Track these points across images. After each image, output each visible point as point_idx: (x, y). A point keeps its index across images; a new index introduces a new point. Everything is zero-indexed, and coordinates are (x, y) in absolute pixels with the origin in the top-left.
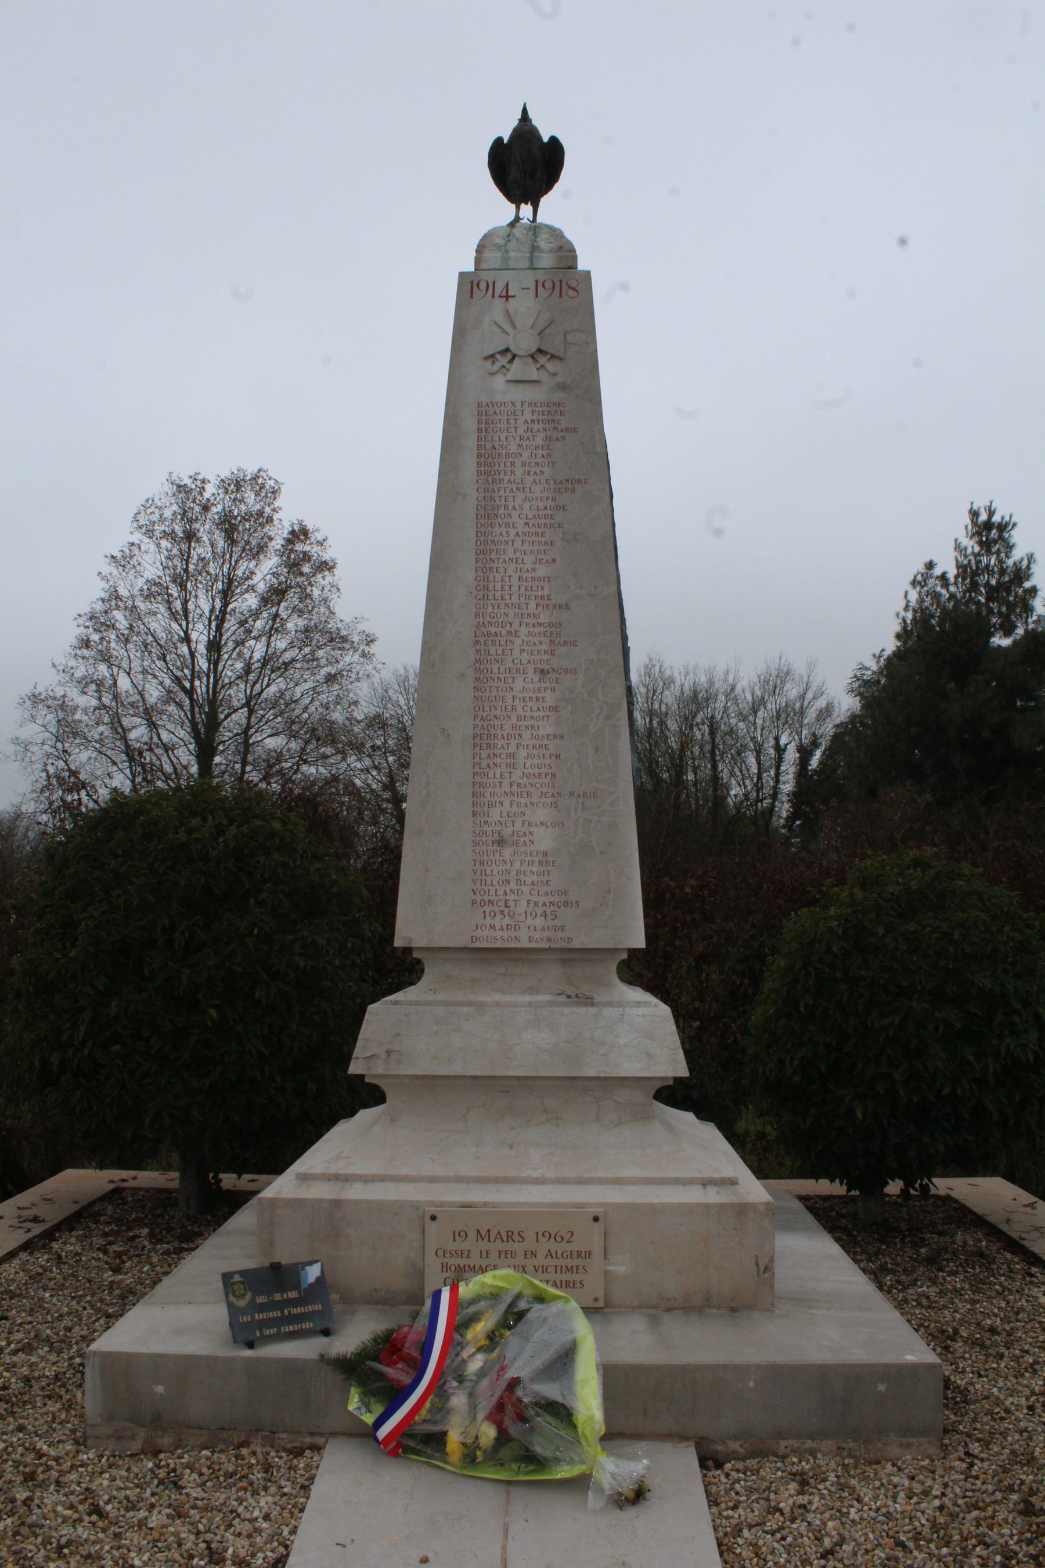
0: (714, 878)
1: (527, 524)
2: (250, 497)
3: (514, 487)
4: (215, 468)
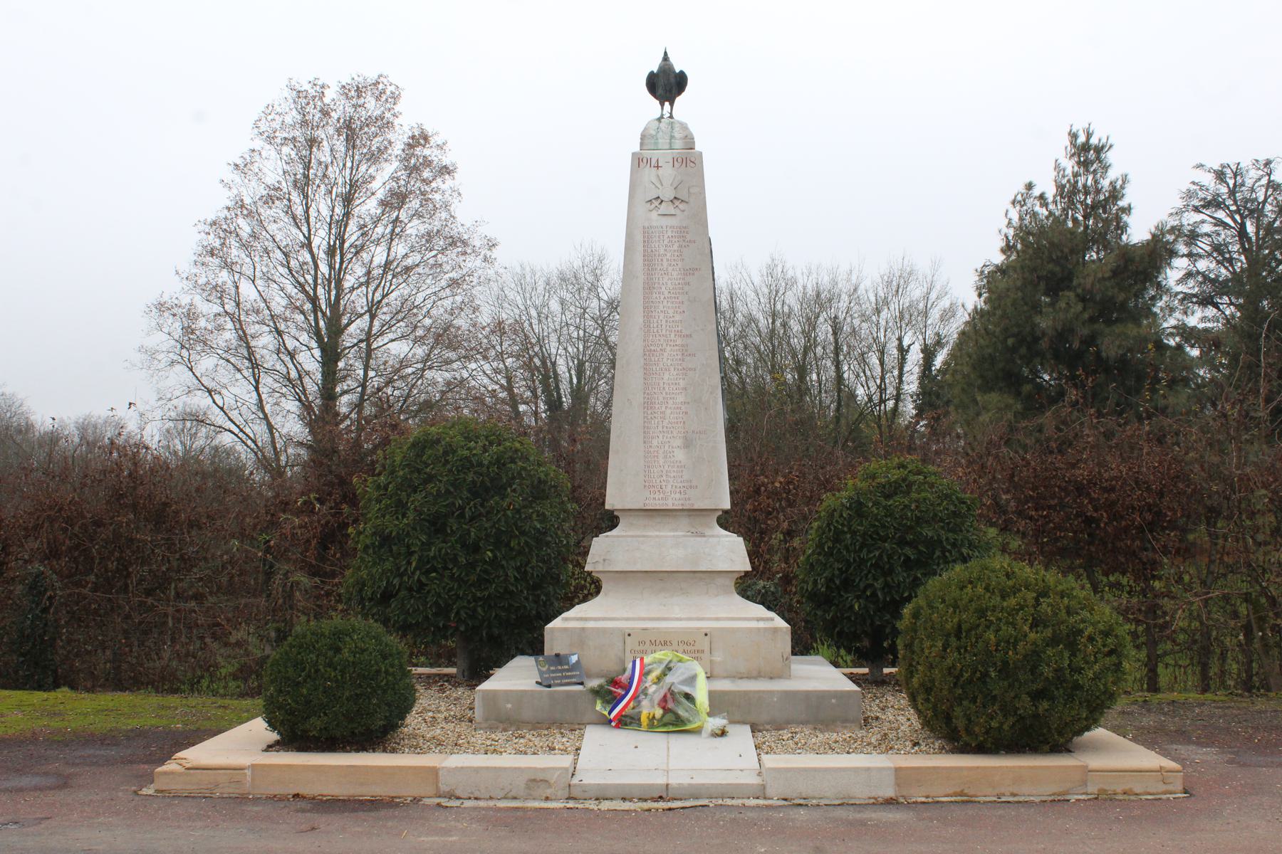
2: (370, 103)
4: (335, 74)
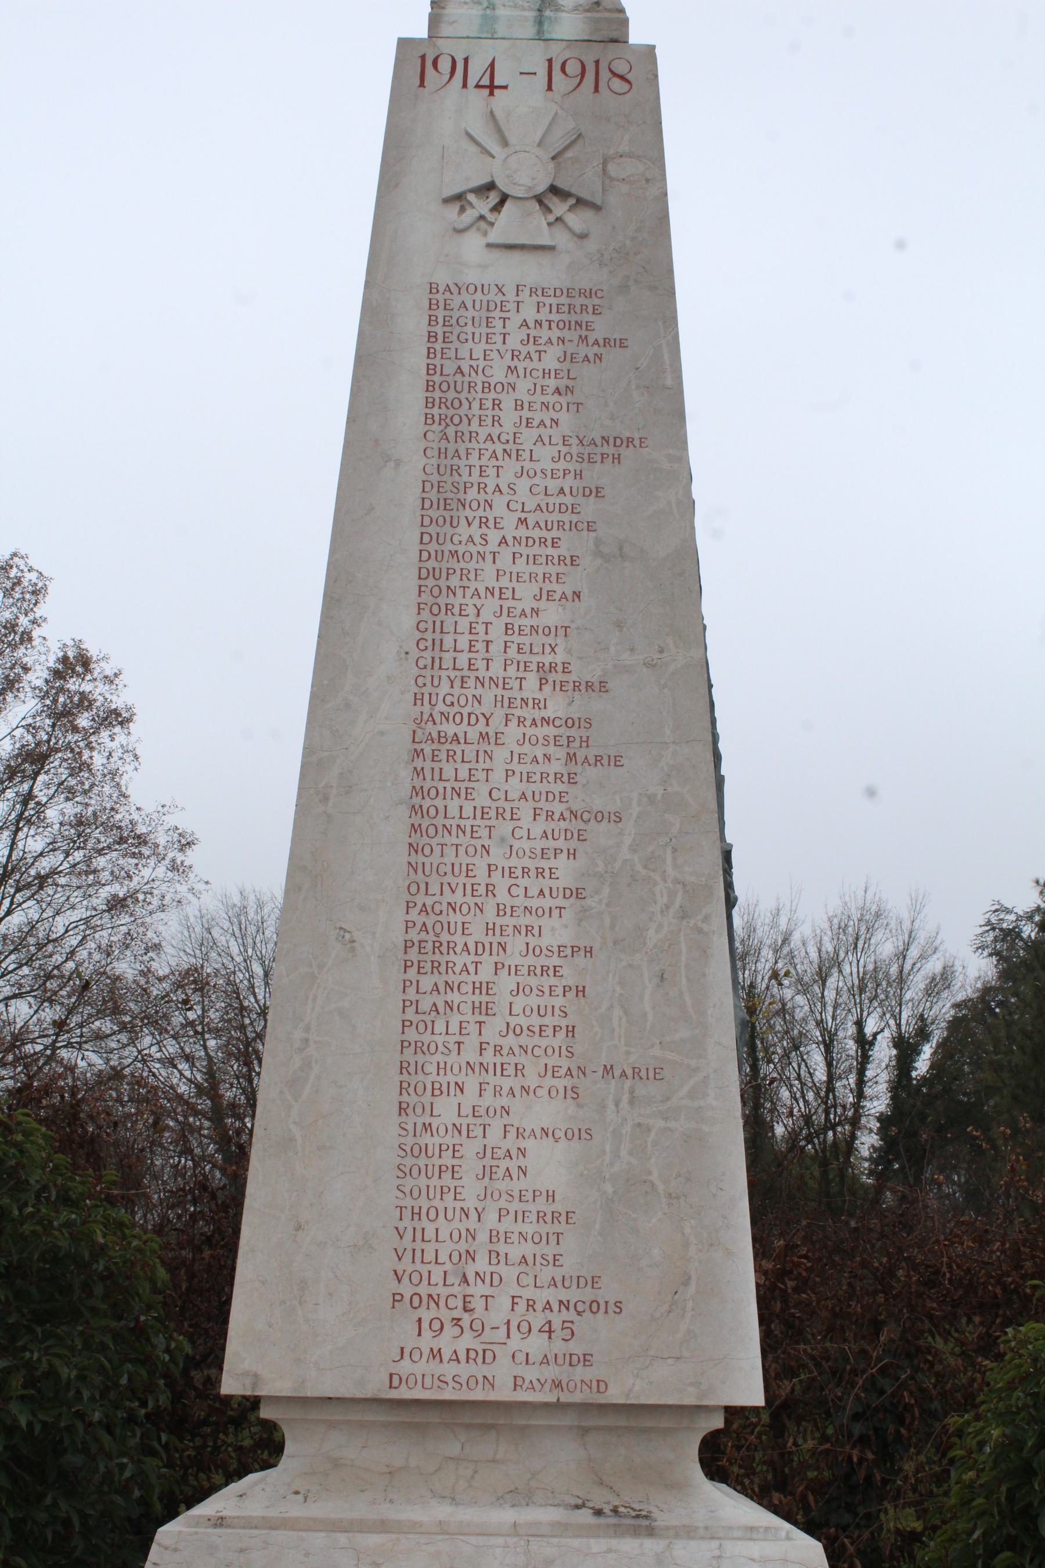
0: (805, 1257)
1: (523, 521)
3: (499, 448)
